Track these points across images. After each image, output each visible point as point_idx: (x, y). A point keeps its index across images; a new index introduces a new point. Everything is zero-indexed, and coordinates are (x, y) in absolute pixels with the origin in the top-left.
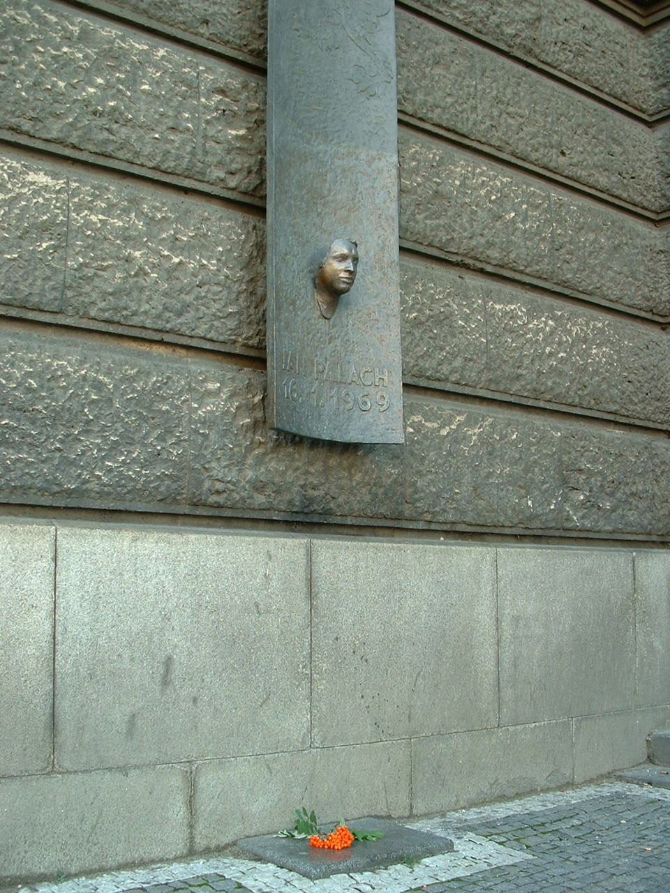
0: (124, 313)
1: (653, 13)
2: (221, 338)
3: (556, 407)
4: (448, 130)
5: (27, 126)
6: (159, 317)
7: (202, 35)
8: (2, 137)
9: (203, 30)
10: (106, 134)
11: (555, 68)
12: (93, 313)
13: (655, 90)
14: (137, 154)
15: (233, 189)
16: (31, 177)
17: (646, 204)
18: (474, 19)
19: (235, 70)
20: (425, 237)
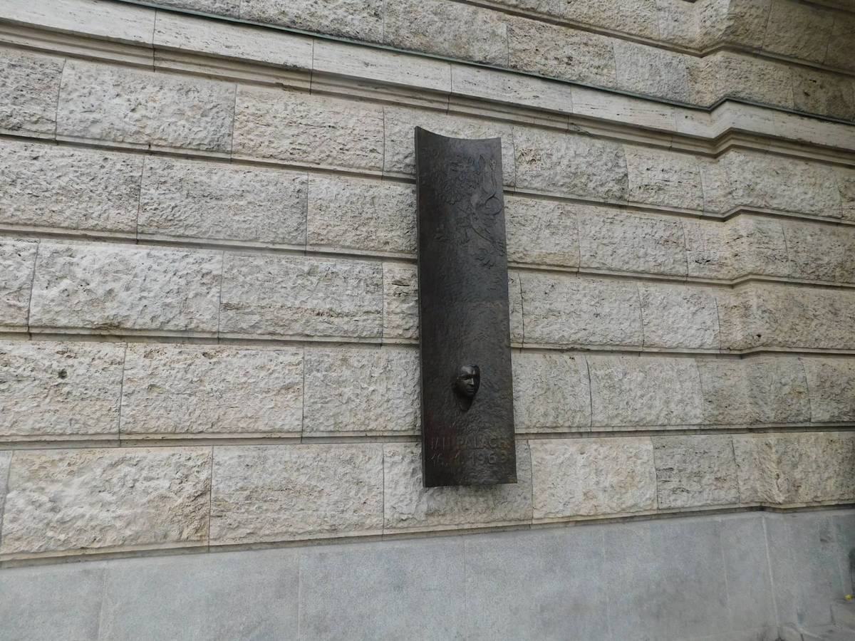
0: (341, 425)
1: (471, 107)
2: (403, 429)
3: (365, 253)
4: (558, 266)
5: (279, 330)
6: (363, 423)
7: (386, 251)
8: (2, 16)
9: (388, 248)
10: (326, 325)
11: (641, 203)
12: (322, 429)
13: (725, 196)
14: (346, 332)
15: (410, 338)
16: (281, 358)
17: (721, 277)
18: (576, 189)
19: (403, 265)
20: (543, 339)
